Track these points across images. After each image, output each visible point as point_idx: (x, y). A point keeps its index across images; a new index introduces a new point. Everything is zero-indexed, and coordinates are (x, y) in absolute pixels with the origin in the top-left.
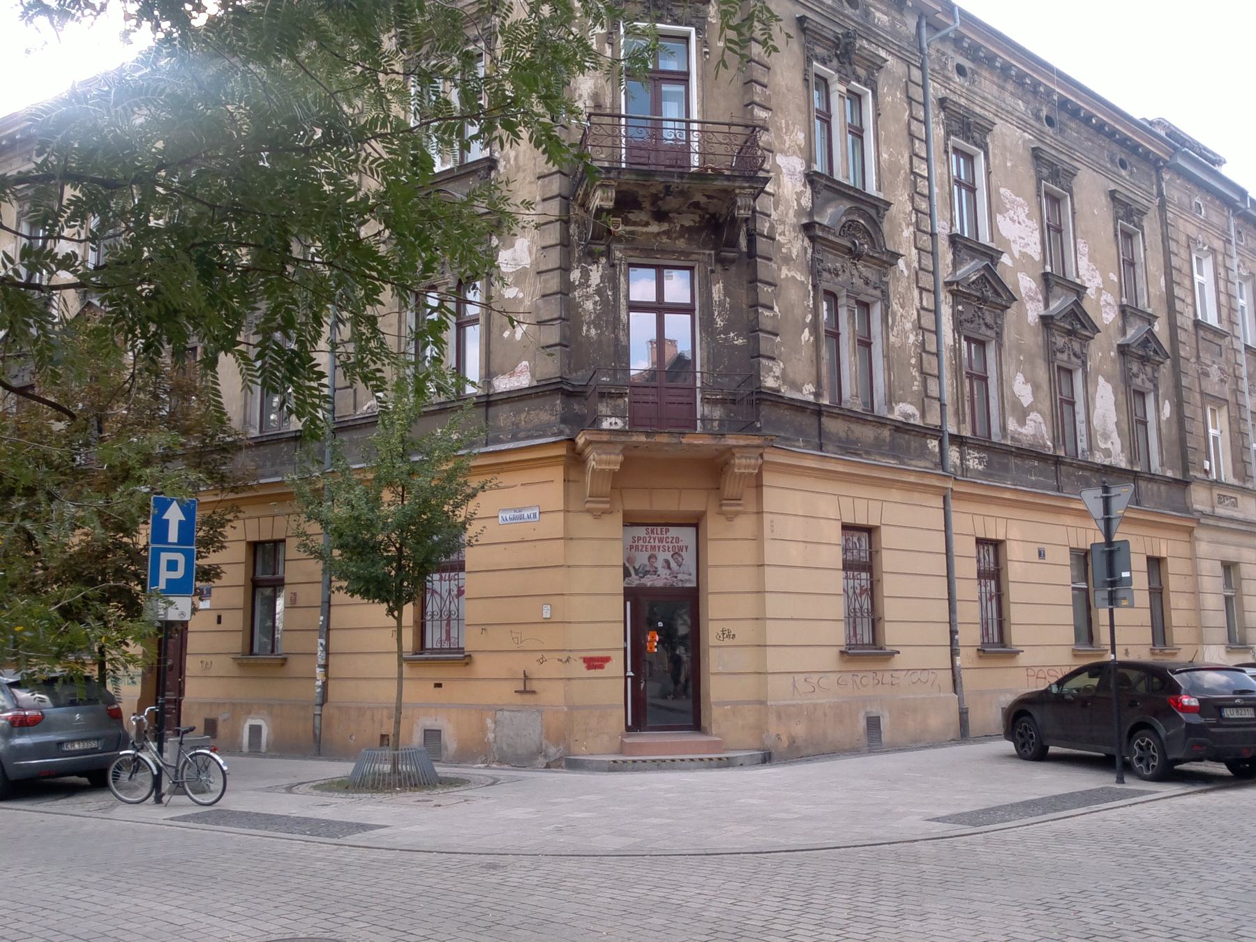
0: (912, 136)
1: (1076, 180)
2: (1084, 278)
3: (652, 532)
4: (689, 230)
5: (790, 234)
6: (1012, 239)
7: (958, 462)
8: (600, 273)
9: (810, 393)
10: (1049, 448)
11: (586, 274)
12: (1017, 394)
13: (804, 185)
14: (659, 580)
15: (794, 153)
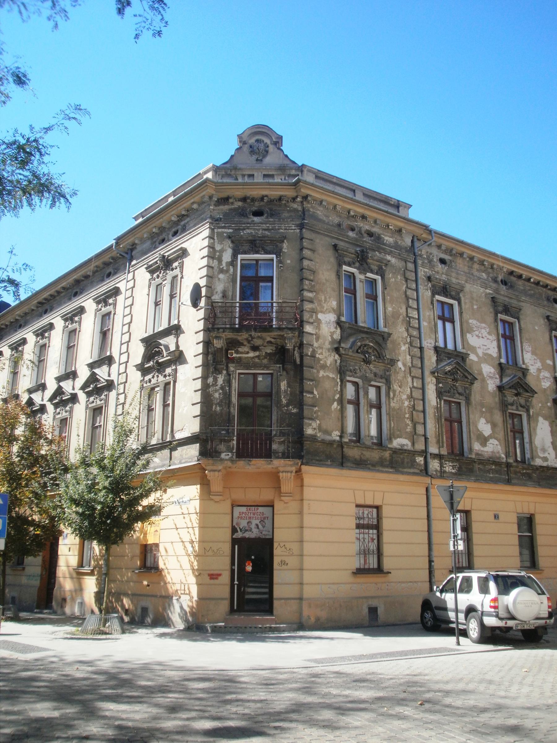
0: (407, 298)
1: (522, 312)
2: (528, 364)
3: (250, 509)
4: (269, 354)
5: (326, 353)
6: (477, 346)
7: (439, 469)
8: (223, 379)
9: (337, 436)
10: (503, 458)
11: (215, 380)
12: (480, 430)
13: (336, 328)
14: (254, 534)
15: (330, 312)
